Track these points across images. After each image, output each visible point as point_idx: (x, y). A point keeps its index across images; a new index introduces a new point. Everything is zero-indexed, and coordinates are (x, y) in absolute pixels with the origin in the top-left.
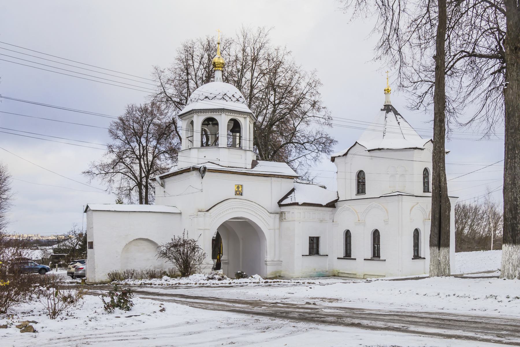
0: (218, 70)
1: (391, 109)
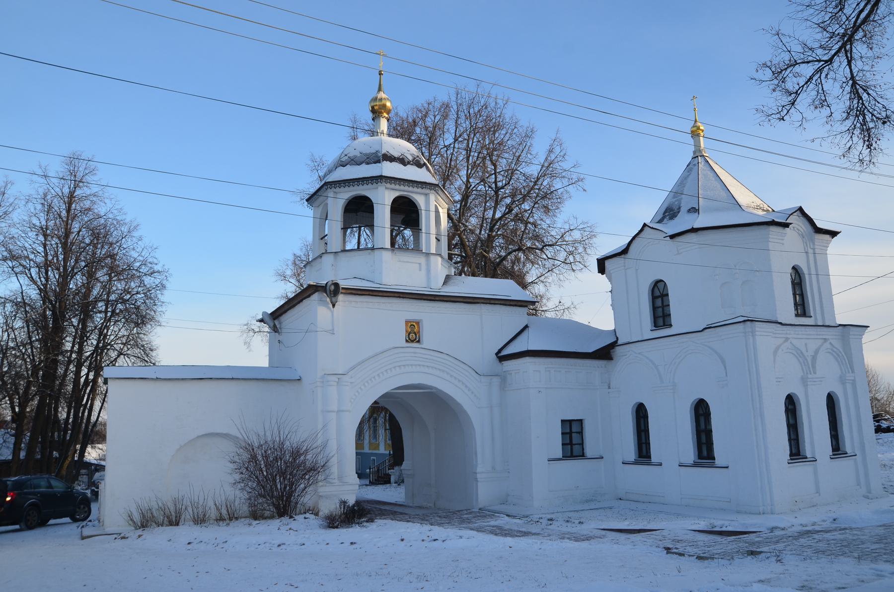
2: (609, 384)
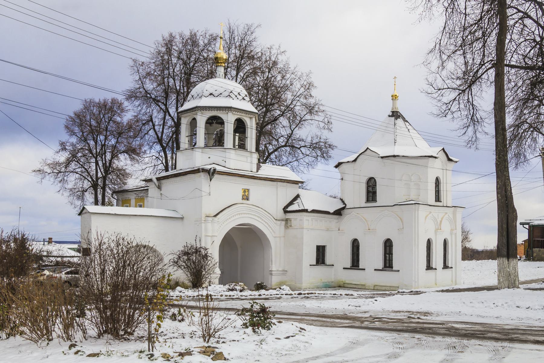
0: (221, 65)
1: (399, 116)
2: (339, 228)
